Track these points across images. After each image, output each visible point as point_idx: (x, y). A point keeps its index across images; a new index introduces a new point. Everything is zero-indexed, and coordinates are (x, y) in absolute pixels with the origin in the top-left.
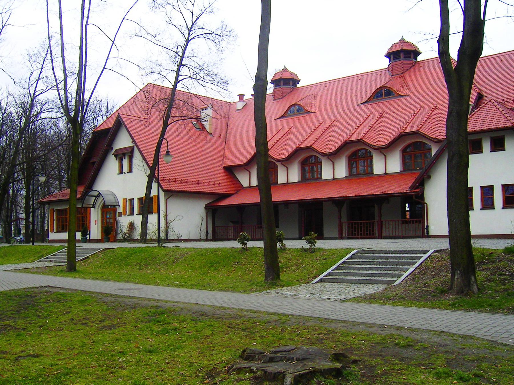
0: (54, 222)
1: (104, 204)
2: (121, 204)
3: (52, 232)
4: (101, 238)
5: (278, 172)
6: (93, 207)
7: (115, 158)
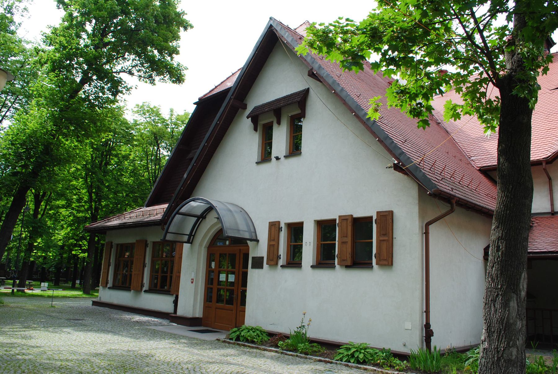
0: (111, 267)
1: (221, 231)
2: (263, 235)
3: (105, 285)
4: (202, 316)
5: (269, 101)
6: (188, 242)
7: (252, 125)
